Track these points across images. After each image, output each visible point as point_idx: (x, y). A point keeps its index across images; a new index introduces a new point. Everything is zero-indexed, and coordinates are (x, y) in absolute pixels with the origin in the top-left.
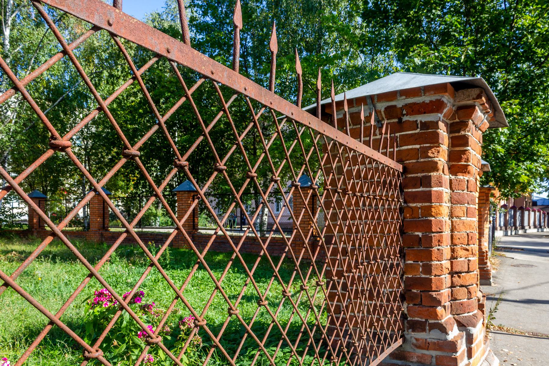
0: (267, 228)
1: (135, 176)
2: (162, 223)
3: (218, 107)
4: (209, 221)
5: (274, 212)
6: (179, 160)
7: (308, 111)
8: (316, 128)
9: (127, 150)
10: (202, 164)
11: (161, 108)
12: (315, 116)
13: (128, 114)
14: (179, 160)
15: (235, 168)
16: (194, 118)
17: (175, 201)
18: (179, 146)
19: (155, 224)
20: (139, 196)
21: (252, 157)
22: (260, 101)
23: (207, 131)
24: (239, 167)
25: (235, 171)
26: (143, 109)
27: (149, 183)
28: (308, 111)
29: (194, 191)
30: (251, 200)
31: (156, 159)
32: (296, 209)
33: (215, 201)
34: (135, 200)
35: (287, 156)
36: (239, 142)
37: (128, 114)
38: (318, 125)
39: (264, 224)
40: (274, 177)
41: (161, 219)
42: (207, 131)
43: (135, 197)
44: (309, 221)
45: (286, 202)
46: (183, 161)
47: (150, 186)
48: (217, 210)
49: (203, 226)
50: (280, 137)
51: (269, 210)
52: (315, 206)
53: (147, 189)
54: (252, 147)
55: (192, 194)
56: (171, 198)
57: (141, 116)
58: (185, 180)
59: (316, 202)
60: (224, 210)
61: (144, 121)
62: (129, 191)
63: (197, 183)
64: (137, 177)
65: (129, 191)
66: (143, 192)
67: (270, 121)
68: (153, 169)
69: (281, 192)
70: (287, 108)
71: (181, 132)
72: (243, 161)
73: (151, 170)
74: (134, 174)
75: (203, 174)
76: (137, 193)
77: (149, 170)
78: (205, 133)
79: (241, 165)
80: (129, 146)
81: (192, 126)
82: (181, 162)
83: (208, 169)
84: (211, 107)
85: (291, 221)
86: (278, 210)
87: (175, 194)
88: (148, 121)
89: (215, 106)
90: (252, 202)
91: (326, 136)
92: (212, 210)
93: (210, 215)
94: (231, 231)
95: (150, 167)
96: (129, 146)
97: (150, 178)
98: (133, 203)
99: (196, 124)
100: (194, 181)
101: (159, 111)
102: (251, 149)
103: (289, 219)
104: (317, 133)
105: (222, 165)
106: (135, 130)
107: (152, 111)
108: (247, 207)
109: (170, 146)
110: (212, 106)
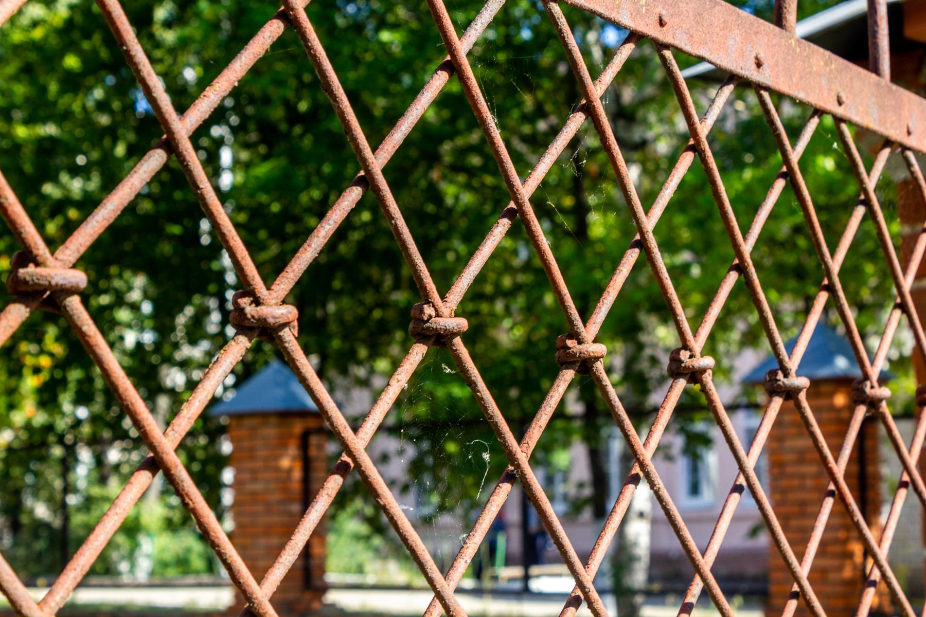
0: (651, 579)
1: (42, 352)
2: (165, 565)
3: (412, 32)
4: (377, 551)
5: (680, 503)
6: (257, 302)
7: (819, 39)
8: (871, 121)
9: (31, 268)
10: (356, 306)
11: (158, 44)
12: (866, 67)
13: (15, 78)
14: (257, 302)
15: (491, 299)
16: (302, 85)
17: (222, 462)
18: (239, 208)
19: (133, 566)
20: (61, 440)
21: (568, 247)
22: (613, 15)
23: (378, 161)
24: (509, 294)
25: (493, 315)
26: (80, 53)
27: (106, 374)
28: (819, 39)
29: (304, 414)
30: (566, 445)
31: (136, 270)
32: (784, 483)
33: (402, 454)
34: (43, 459)
35: (739, 254)
36: (520, 205)
37: (15, 78)
38: (881, 107)
39: (632, 559)
40: (684, 355)
41: (154, 546)
42: (378, 161)
43: (44, 445)
44: (845, 541)
45: (742, 469)
46: (276, 305)
47: (112, 393)
48: (411, 497)
49: (347, 571)
50: (708, 170)
51: (657, 493)
52: (870, 469)
53: (97, 407)
54: (568, 202)
55: (298, 427)
56: (205, 448)
57: (73, 83)
58: (266, 363)
59: (875, 449)
60: (444, 496)
61: (84, 107)
62: (18, 418)
63: (321, 373)
64: (51, 355)
65: (18, 418)
66: (78, 423)
67: (646, 79)
68: (123, 315)
69: (711, 407)
70: (735, 40)
71: (247, 146)
72: (527, 267)
73: (114, 323)
74: (39, 340)
75: (348, 334)
76: (49, 428)
77: (104, 319)
78: (368, 171)
79: (517, 289)
80: (41, 248)
81: (293, 117)
82: (263, 311)
83: (370, 310)
84: (378, 29)
85: (763, 540)
86: (695, 489)
87: (222, 430)
88: (102, 106)
89: (394, 27)
90: (573, 459)
91: (917, 153)
92: (388, 497)
93: (380, 524)
94: (477, 592)
95: (110, 308)
96: (41, 248)
97: (113, 361)
98: (37, 474)
99: (315, 110)
100: (308, 365)
101: (153, 61)
102: (563, 211)
103: (754, 532)
104: (876, 143)
105: (446, 313)
106: (46, 147)
107: (121, 61)
108: (549, 482)
109: (200, 209)
110: (382, 24)
